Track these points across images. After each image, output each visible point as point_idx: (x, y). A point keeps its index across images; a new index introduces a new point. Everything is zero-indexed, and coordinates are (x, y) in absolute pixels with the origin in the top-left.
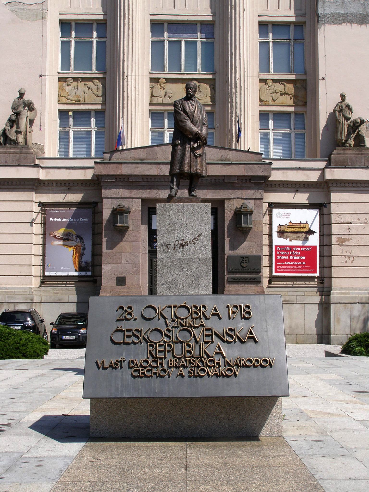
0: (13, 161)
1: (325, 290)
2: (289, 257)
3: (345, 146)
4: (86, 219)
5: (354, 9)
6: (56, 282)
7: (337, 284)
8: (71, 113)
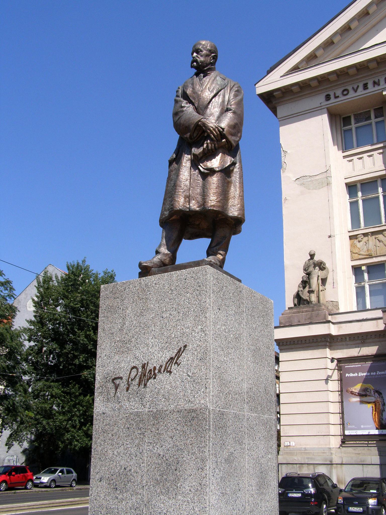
0: (305, 319)
6: (357, 442)
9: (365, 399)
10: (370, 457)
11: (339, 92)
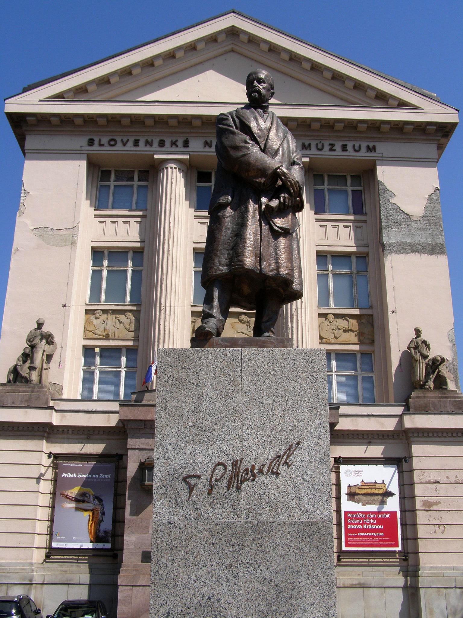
0: (22, 401)
1: (410, 569)
2: (363, 527)
3: (425, 389)
4: (107, 476)
5: (421, 238)
6: (65, 557)
7: (427, 562)
8: (97, 350)
9: (82, 505)
10: (78, 575)
11: (105, 140)
